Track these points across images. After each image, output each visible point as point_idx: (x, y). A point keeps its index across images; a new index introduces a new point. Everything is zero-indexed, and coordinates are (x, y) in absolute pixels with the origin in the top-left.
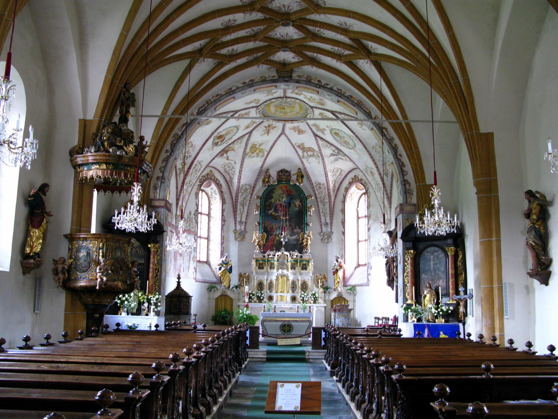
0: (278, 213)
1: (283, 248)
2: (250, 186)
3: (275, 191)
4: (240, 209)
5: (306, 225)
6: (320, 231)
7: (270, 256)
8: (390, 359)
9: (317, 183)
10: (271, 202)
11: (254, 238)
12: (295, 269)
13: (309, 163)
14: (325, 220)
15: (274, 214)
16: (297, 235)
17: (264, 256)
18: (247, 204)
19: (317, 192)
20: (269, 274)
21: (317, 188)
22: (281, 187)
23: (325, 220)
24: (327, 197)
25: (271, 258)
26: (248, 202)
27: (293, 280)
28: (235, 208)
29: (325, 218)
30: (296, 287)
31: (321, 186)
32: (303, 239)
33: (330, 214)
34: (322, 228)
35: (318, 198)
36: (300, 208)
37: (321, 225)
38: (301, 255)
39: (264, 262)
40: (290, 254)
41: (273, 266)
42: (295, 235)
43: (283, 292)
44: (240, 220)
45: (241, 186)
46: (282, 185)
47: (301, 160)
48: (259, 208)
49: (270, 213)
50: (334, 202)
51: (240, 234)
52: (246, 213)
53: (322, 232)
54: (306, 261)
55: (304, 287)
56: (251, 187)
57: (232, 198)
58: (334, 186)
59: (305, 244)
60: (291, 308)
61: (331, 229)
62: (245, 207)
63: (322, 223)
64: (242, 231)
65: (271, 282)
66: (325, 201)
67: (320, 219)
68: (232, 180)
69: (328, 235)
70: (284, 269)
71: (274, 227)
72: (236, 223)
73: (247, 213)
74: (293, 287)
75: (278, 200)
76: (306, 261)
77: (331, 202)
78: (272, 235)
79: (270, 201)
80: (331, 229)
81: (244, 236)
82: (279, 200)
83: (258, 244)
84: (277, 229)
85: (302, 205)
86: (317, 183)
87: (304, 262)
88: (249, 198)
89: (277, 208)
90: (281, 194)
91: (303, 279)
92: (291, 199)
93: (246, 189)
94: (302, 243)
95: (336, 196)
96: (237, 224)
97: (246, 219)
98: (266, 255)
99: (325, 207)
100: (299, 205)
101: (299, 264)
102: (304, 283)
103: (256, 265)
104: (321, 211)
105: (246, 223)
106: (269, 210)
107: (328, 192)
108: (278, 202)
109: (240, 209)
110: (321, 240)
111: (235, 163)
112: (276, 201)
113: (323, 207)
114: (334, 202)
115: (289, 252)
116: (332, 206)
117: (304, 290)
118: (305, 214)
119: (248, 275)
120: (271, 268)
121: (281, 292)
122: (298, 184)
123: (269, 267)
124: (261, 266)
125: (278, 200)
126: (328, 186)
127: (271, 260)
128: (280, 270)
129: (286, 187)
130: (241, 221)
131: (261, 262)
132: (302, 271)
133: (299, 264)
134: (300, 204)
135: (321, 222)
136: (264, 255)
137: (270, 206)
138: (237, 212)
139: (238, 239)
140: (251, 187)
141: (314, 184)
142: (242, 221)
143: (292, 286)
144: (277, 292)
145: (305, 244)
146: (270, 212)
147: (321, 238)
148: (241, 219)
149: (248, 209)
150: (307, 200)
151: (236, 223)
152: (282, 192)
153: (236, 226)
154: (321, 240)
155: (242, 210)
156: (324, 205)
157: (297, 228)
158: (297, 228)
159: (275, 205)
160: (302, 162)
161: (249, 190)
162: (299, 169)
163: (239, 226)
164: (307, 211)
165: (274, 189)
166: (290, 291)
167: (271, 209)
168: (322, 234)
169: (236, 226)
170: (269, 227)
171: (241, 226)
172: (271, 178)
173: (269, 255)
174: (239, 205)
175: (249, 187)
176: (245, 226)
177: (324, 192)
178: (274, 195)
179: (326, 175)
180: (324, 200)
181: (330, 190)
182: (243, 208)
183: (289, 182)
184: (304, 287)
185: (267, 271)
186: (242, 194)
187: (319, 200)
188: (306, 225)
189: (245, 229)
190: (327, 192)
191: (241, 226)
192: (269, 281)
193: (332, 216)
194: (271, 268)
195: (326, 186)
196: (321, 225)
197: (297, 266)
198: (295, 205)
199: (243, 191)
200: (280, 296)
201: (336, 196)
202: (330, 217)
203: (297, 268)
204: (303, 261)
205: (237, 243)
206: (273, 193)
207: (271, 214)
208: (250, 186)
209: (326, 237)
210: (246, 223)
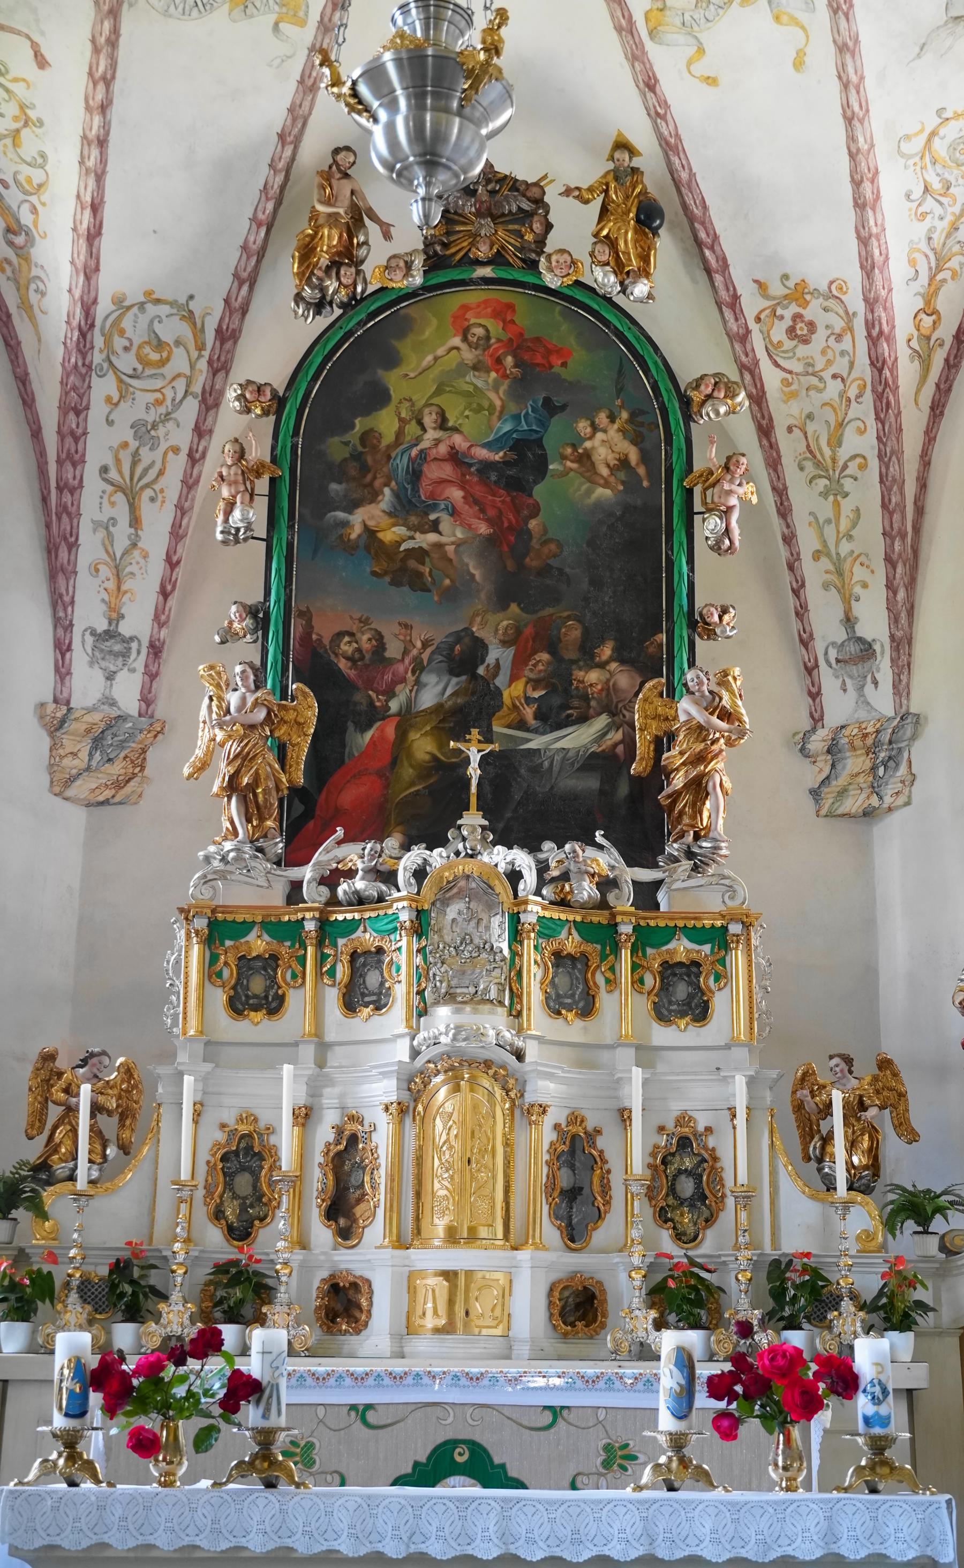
0: (435, 527)
1: (472, 820)
2: (190, 317)
3: (405, 347)
4: (107, 526)
5: (682, 631)
6: (807, 724)
7: (343, 888)
8: (510, 1389)
9: (777, 289)
10: (368, 437)
11: (203, 736)
12: (587, 1009)
13: (711, 81)
14: (849, 621)
15: (391, 533)
16: (602, 721)
17: (295, 892)
18: (172, 484)
19: (771, 378)
20: (336, 1058)
21: (779, 333)
22: (465, 308)
23: (849, 621)
24: (865, 409)
25: (360, 900)
26: (178, 464)
27: (575, 1118)
28: (64, 509)
29: (848, 599)
30: (606, 1188)
31: (813, 311)
32: (662, 743)
33: (889, 560)
34: (815, 695)
35: (780, 433)
36: (632, 484)
37: (810, 670)
38: (646, 875)
39: (285, 949)
40: (542, 868)
41: (372, 979)
42: (583, 719)
43: (473, 1238)
44: (102, 625)
45: (104, 307)
46: (473, 297)
47: (636, 56)
48: (263, 485)
49: (356, 532)
50: (925, 461)
51: (97, 742)
52: (156, 568)
53: (817, 719)
54: (698, 934)
55: (687, 1187)
56: (199, 331)
57: (36, 433)
58: (929, 309)
59: (679, 781)
60: (556, 1412)
61: (901, 689)
62: (147, 509)
63: (819, 646)
64: (122, 718)
65: (353, 1139)
66: (844, 453)
67: (801, 612)
68: (23, 253)
69: (871, 750)
70: (478, 1000)
71: (393, 650)
72: (62, 648)
73: (172, 563)
74: (572, 1194)
75: (429, 420)
76: (698, 934)
77: (898, 453)
78: (373, 715)
79: (360, 425)
80: (901, 689)
81: (139, 762)
82: (442, 424)
83: (232, 786)
84: (419, 668)
85: (645, 458)
86: (777, 289)
87: (682, 948)
88: (182, 437)
89: (425, 487)
90: (462, 369)
91: (676, 1107)
92: (550, 408)
93: (160, 345)
94: (660, 773)
95: (937, 409)
96: (79, 658)
97: (160, 619)
98: (307, 873)
99: (847, 506)
100: (624, 463)
101: (626, 954)
102: (684, 1143)
103: (211, 973)
104: (807, 542)
105: (156, 649)
106: (352, 506)
107: (877, 364)
108: (431, 435)
109: (107, 526)
110: (815, 793)
111: (41, 62)
112: (412, 429)
113: (825, 509)
114: (925, 461)
115: (533, 848)
116: (910, 489)
117: (686, 1219)
118: (680, 536)
119: (128, 1071)
120: (350, 1005)
121: (452, 1237)
122: (606, 280)
123: (332, 996)
124: (257, 985)
125: (429, 420)
126: (871, 303)
127: (350, 927)
128: (443, 1014)
129: (503, 312)
130: (110, 635)
131: (258, 943)
132: (662, 1035)
133: (626, 954)
134: (633, 456)
135: (806, 641)
136: (294, 873)
137: (364, 469)
138: (73, 546)
139: (81, 788)
140: (199, 331)
141: (751, 304)
142: (125, 629)
143: (565, 1179)
144: (401, 1244)
145: (679, 781)
146: (358, 519)
147: (812, 775)
148: (116, 616)
149: (177, 534)
150: (688, 418)
151: (62, 648)
152: (469, 355)
153: (62, 672)
154: (815, 793)
155: (122, 531)
156: (836, 491)
157: (606, 651)
158: (606, 651)
159: (401, 463)
160: (650, 84)
161: (179, 362)
162: (622, 145)
163: (98, 676)
164: (689, 515)
165: (402, 327)
166: (550, 1232)
167: (374, 496)
168: (817, 742)
169: (62, 672)
170: (346, 647)
171: (110, 677)
172: (372, 228)
173: (330, 880)
174: (93, 486)
175: (185, 330)
176: (152, 676)
177: (841, 366)
178: (393, 380)
179: (857, 183)
180: (836, 441)
181: (890, 339)
182: (135, 522)
183: (533, 266)
184: (687, 1187)
185: (318, 1032)
186: (124, 391)
187: (790, 447)
188: (682, 631)
189: (147, 699)
190: (863, 359)
191: (110, 677)
192: (324, 1134)
193: (912, 583)
194: (350, 1005)
195: (856, 303)
196: (810, 670)
197: (612, 983)
198: (585, 459)
199: (126, 363)
200: (441, 1284)
201: (937, 409)
202: (891, 587)
203: (606, 1001)
204: (671, 933)
205: (77, 816)
206: (392, 360)
207: (370, 533)
208: (190, 317)
209: (855, 763)
210: (156, 649)
